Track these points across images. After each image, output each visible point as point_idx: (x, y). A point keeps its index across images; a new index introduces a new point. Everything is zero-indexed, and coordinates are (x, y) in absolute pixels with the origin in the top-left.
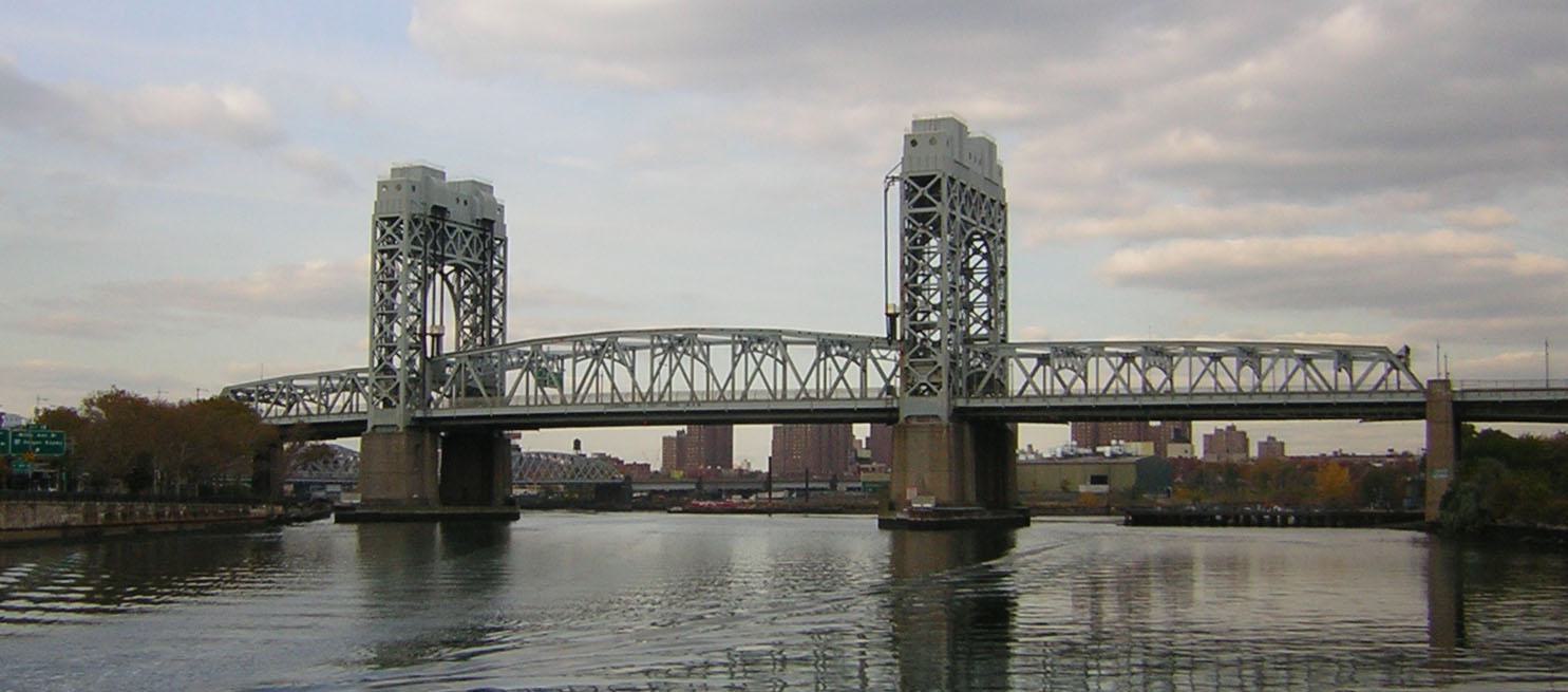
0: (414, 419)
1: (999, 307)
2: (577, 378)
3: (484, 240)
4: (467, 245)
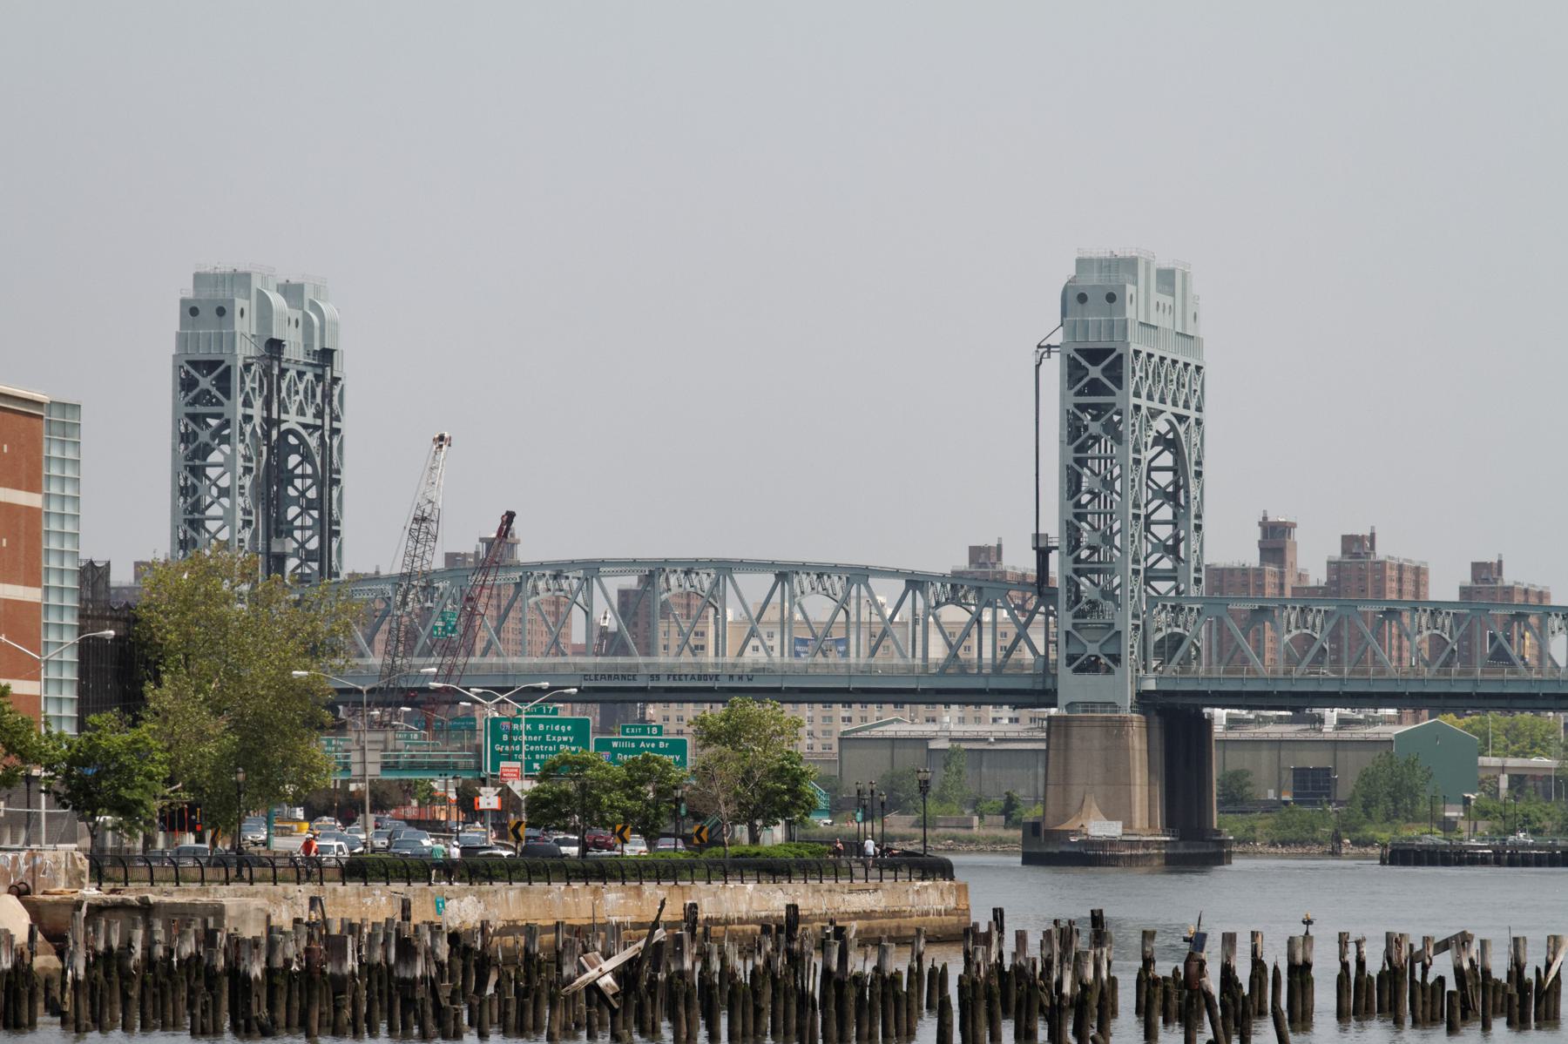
2: (779, 601)
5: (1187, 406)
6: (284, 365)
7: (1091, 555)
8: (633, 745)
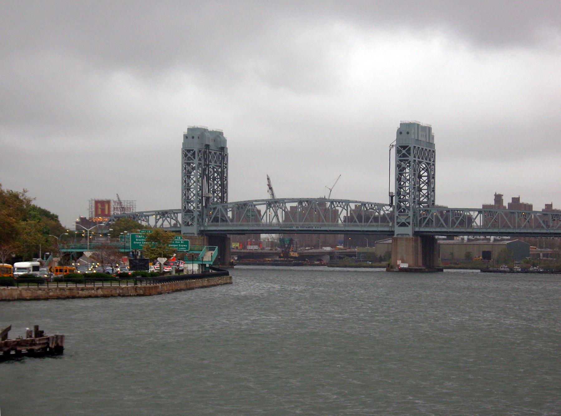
0: (200, 231)
1: (432, 191)
5: (430, 160)
6: (210, 151)
7: (404, 197)
8: (179, 242)
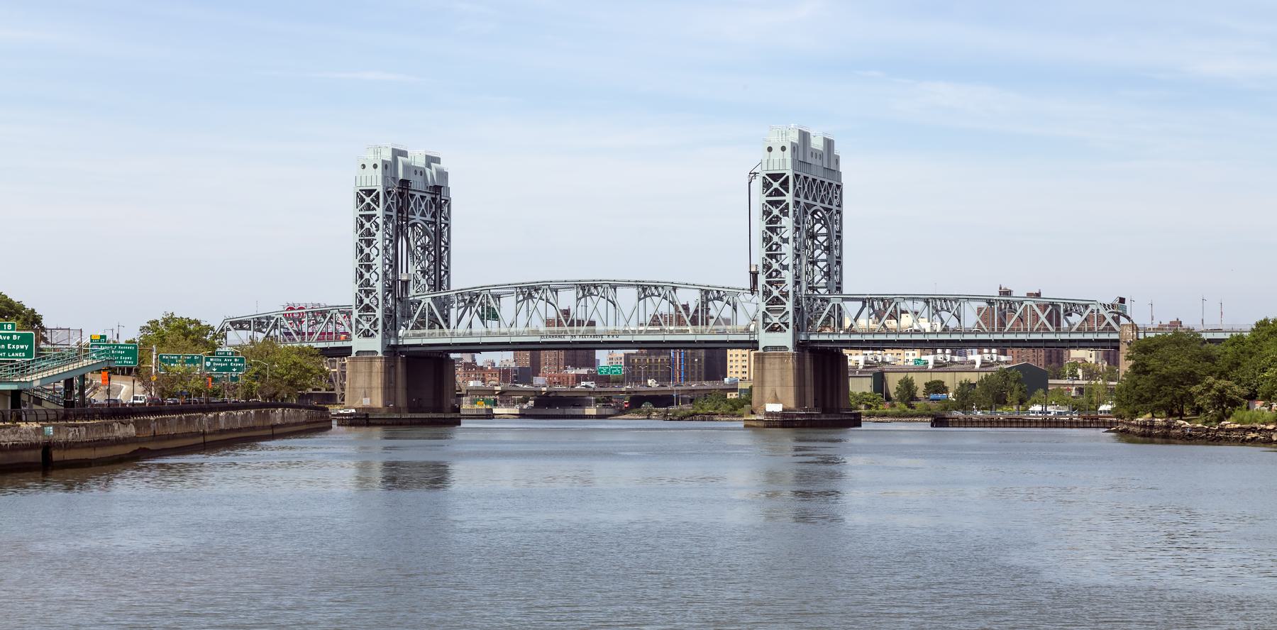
3: (435, 203)
4: (423, 207)
5: (830, 203)
